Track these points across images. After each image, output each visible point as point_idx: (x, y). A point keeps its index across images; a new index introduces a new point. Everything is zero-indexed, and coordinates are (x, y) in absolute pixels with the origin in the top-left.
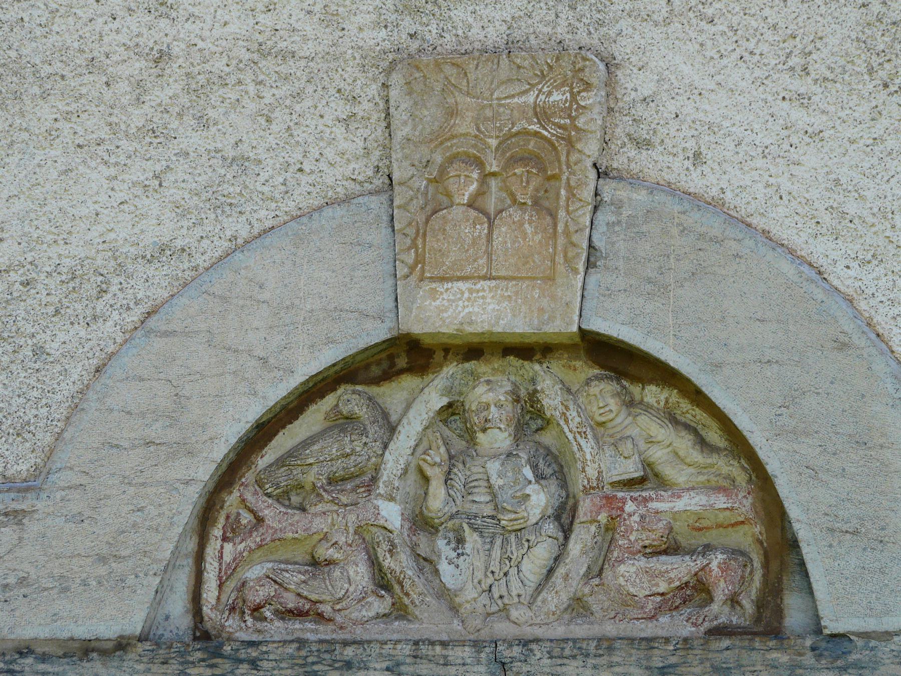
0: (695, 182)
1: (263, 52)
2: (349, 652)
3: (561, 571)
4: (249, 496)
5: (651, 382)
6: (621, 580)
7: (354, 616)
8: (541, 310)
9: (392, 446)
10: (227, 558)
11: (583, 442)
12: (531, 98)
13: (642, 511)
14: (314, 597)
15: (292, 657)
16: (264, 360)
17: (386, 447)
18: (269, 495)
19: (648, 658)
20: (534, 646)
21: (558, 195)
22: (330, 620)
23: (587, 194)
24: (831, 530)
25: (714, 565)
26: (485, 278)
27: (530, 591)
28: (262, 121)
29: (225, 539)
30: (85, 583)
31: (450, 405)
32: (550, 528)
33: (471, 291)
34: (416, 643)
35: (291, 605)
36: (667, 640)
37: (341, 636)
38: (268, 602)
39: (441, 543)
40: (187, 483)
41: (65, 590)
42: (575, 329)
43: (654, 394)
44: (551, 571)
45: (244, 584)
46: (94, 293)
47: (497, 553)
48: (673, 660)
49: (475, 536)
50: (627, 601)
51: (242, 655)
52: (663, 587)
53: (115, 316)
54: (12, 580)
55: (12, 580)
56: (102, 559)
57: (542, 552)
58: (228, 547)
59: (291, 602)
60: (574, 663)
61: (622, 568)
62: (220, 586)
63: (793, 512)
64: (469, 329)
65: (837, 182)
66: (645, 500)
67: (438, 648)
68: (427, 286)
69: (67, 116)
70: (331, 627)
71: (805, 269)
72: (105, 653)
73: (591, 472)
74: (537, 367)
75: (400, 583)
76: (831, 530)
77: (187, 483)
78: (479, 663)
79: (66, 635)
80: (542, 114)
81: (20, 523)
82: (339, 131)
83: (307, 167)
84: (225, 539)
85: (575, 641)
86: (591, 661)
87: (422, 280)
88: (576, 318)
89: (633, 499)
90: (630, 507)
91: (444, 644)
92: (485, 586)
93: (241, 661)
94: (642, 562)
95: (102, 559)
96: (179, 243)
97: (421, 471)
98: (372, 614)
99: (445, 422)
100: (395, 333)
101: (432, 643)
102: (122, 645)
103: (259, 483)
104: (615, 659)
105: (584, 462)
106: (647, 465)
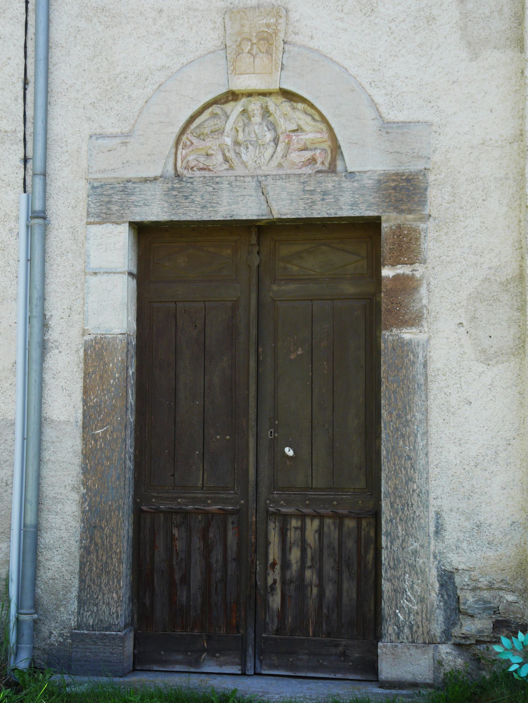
0: (311, 44)
1: (189, 9)
2: (218, 179)
3: (275, 156)
4: (189, 137)
5: (299, 102)
6: (292, 158)
7: (219, 169)
8: (269, 83)
9: (228, 122)
10: (184, 154)
11: (281, 120)
12: (265, 21)
13: (297, 138)
14: (208, 164)
15: (202, 181)
16: (192, 98)
17: (226, 122)
18: (194, 136)
19: (300, 179)
20: (268, 177)
21: (273, 49)
22: (212, 171)
23: (281, 49)
24: (350, 143)
25: (317, 153)
26: (253, 74)
27: (267, 161)
28: (190, 29)
29: (183, 149)
30: (145, 162)
31: (244, 110)
32: (272, 144)
33: (249, 77)
34: (236, 177)
35: (201, 167)
36: (305, 174)
37: (215, 175)
38: (195, 166)
39: (242, 149)
40: (172, 133)
41: (139, 164)
42: (278, 88)
43: (300, 106)
44: (272, 156)
45: (188, 161)
46: (144, 80)
47: (257, 151)
48: (306, 180)
49: (252, 146)
50: (294, 164)
51: (189, 181)
52: (303, 160)
53: (150, 86)
54: (125, 161)
55: (125, 161)
56: (149, 155)
57: (270, 151)
58: (184, 151)
59: (201, 166)
60: (279, 181)
61: (292, 155)
62: (182, 162)
63: (339, 138)
64: (249, 88)
65: (351, 43)
66: (298, 136)
67: (242, 178)
68: (237, 76)
69: (135, 29)
70: (212, 172)
71: (342, 69)
72: (151, 181)
73: (283, 128)
74: (268, 99)
75: (231, 160)
76: (350, 143)
77: (172, 133)
78: (253, 182)
79: (140, 176)
80: (268, 26)
81: (126, 145)
82: (211, 32)
83: (202, 43)
84: (183, 149)
85: (279, 175)
86: (284, 181)
87: (235, 74)
88: (278, 85)
89: (295, 135)
90: (294, 137)
91: (244, 177)
92: (254, 160)
93: (188, 183)
94: (297, 153)
95: (149, 155)
96: (167, 65)
97: (236, 129)
98: (224, 169)
99: (243, 115)
100: (228, 90)
101: (240, 177)
102: (155, 179)
103: (192, 133)
104: (290, 180)
105: (281, 125)
106: (299, 126)
